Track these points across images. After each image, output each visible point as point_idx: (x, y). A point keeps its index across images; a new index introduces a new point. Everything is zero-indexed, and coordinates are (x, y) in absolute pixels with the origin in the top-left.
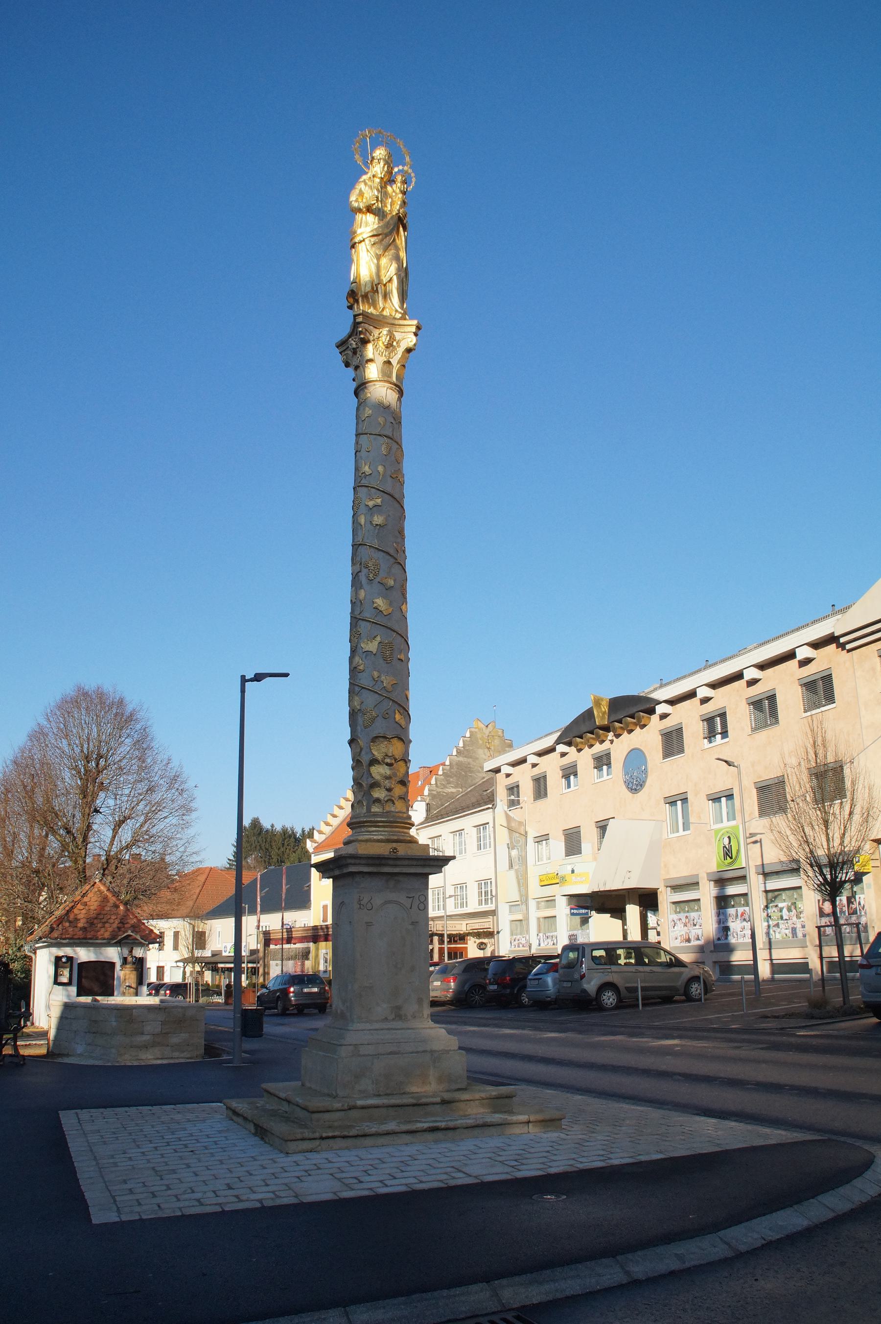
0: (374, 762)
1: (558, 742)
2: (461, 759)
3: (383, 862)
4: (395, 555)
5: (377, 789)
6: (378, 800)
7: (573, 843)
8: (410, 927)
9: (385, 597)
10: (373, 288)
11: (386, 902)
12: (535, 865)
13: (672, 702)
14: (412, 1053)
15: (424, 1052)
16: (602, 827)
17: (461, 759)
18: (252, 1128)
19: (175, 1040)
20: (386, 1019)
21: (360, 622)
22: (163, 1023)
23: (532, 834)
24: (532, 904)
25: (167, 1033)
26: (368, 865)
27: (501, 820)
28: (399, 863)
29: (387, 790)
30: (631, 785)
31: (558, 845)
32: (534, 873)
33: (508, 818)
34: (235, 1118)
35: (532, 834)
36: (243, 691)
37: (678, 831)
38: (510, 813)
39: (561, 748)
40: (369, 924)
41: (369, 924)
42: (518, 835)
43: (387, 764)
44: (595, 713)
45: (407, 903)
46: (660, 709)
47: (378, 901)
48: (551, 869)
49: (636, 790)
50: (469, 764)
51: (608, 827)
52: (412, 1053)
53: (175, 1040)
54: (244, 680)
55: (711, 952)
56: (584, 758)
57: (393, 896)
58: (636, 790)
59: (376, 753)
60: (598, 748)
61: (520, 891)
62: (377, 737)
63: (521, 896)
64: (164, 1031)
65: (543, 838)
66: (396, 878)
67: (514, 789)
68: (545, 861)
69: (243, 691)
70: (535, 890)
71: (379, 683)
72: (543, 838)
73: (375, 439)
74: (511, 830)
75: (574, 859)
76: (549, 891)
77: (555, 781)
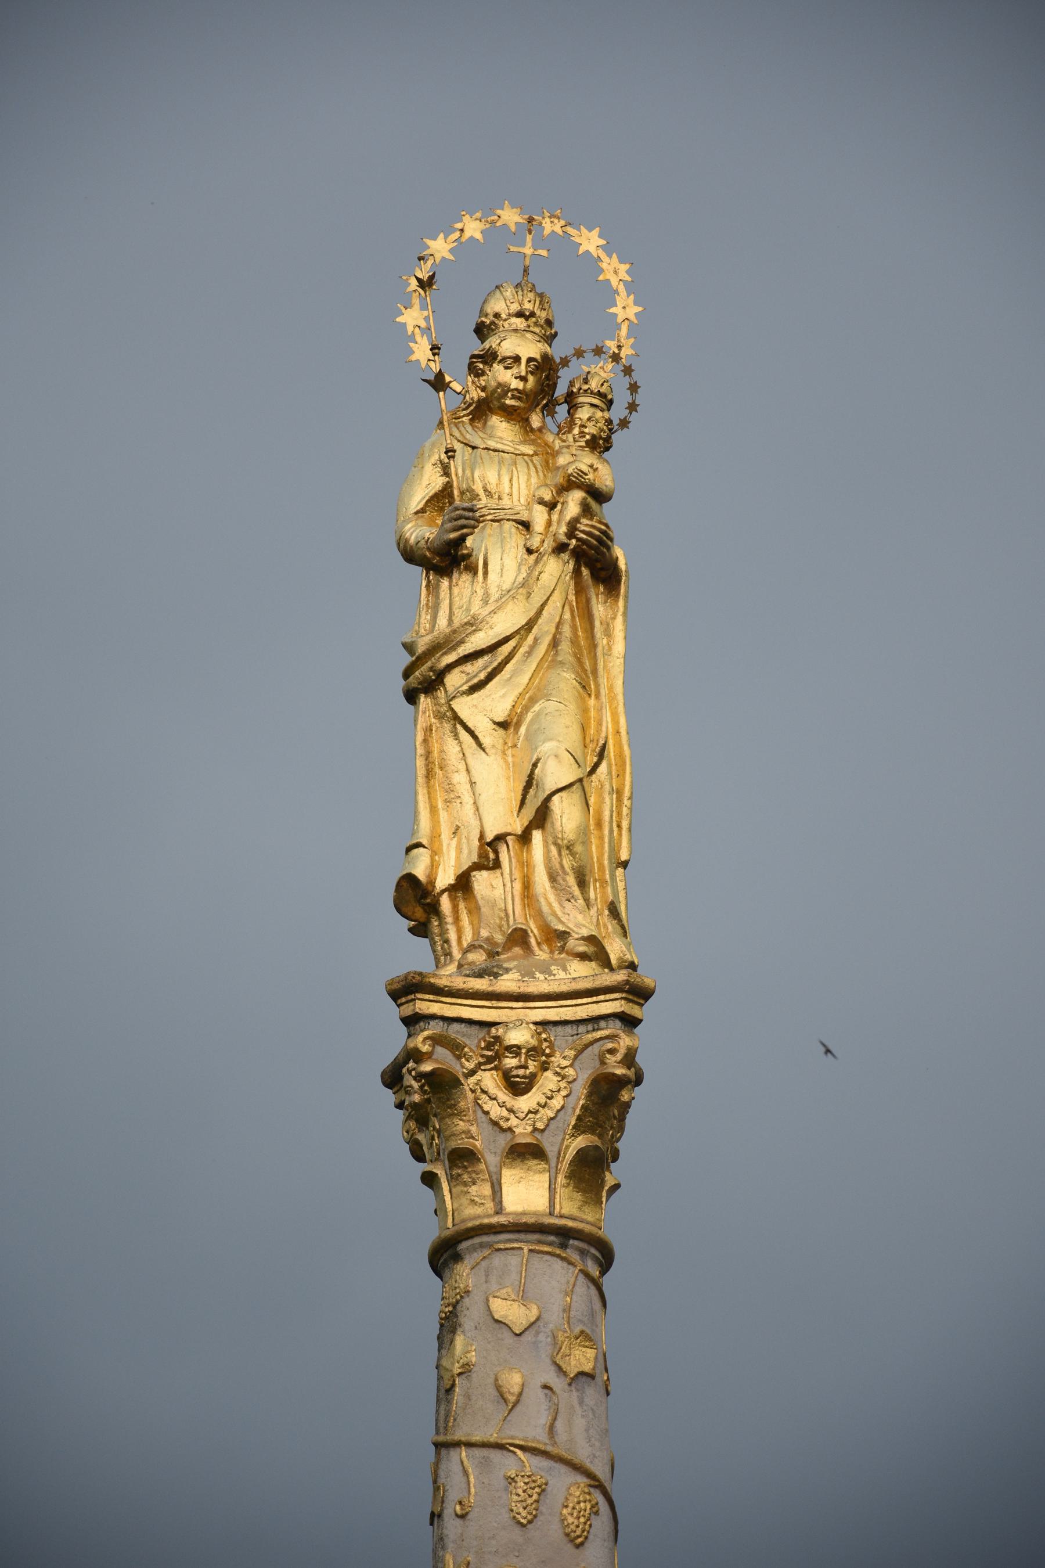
10: (483, 855)
73: (485, 1465)
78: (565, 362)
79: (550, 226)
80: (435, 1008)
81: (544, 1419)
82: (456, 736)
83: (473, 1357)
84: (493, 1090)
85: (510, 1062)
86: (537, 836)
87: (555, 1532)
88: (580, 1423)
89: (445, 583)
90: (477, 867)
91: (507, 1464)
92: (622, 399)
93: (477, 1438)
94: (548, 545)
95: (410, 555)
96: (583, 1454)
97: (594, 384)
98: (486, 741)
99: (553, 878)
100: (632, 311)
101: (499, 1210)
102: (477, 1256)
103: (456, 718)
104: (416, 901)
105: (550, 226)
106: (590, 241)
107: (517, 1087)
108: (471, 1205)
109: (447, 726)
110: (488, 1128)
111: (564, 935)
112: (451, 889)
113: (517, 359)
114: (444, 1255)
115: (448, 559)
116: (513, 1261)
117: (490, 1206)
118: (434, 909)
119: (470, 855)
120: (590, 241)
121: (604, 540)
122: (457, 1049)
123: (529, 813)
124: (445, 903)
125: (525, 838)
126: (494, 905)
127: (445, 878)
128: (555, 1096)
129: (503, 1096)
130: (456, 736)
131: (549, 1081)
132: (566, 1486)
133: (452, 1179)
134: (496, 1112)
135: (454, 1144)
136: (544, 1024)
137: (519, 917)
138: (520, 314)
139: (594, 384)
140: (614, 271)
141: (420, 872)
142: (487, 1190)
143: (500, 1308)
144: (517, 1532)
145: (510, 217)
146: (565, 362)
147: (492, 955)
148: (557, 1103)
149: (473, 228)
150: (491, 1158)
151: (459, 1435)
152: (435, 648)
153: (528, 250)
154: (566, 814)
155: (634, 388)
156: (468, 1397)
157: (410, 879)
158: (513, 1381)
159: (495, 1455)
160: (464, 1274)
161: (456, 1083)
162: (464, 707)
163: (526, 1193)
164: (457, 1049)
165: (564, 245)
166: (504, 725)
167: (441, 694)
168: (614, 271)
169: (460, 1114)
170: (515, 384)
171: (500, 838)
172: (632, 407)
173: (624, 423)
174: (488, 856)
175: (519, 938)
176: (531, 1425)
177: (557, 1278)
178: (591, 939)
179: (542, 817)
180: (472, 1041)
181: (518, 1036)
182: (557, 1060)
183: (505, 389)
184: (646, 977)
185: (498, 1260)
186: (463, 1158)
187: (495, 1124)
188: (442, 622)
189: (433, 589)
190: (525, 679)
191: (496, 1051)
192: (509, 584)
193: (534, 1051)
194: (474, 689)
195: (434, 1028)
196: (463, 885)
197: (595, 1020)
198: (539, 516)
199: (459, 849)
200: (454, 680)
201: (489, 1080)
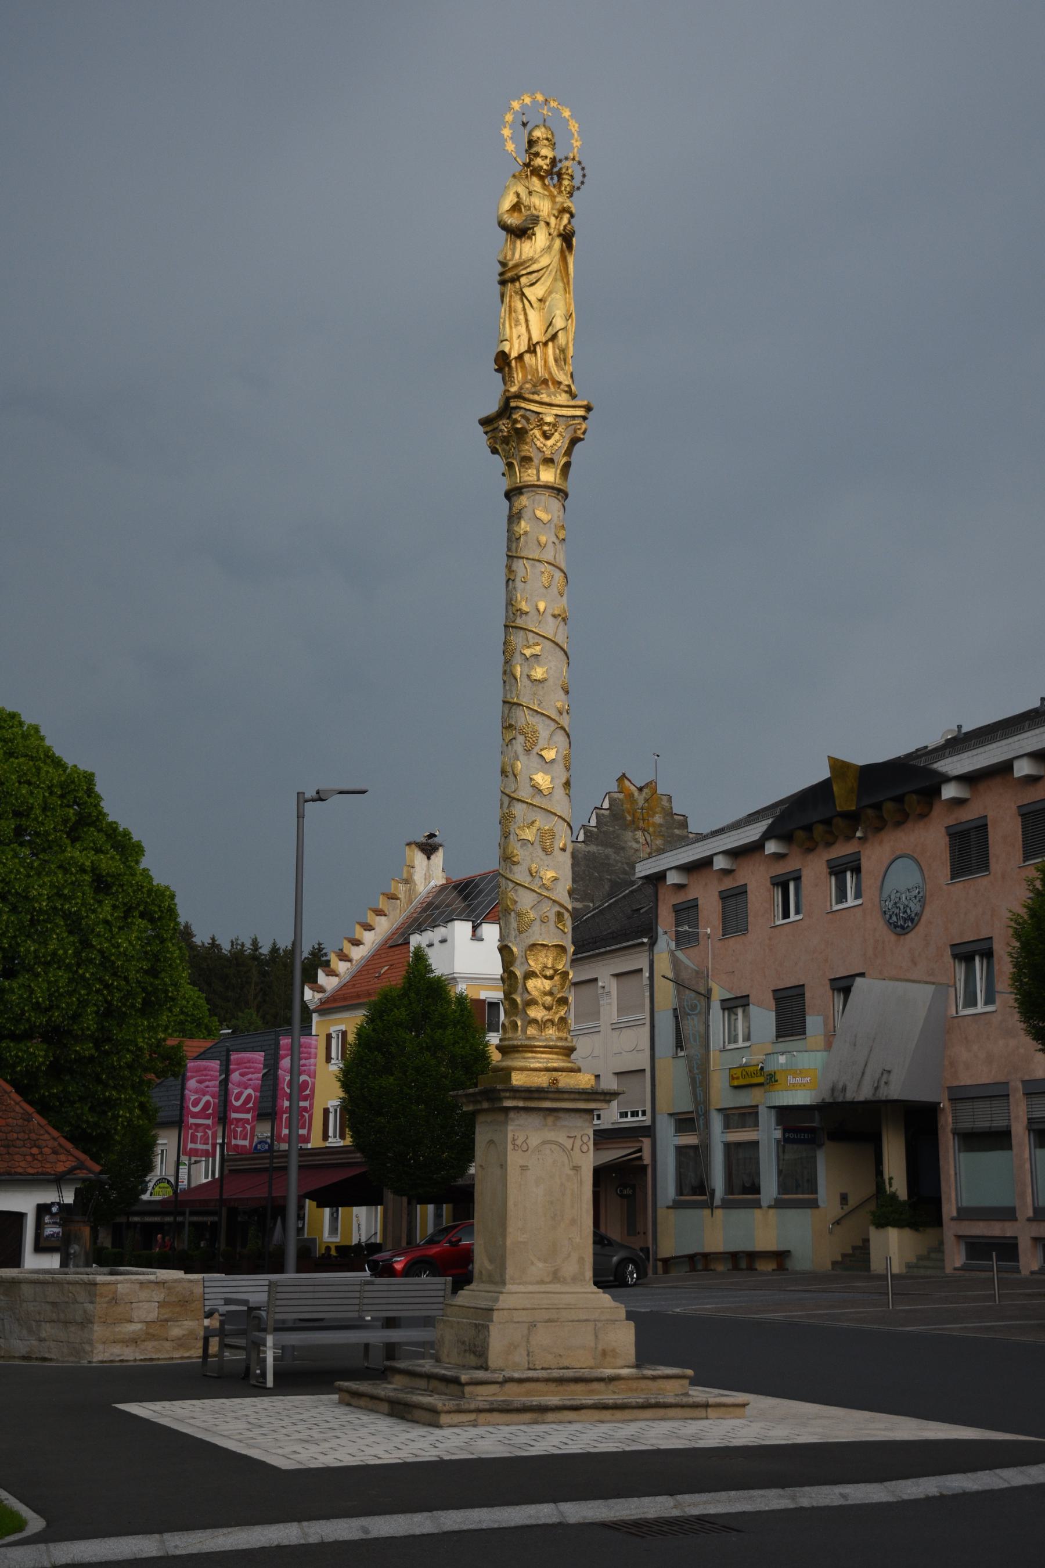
0: (530, 975)
1: (766, 836)
2: (593, 848)
3: (542, 1095)
4: (557, 719)
5: (533, 1007)
6: (534, 1021)
7: (791, 1012)
8: (571, 1173)
9: (546, 773)
10: (529, 347)
11: (544, 1143)
12: (724, 1050)
13: (970, 779)
14: (573, 1321)
15: (586, 1320)
16: (843, 987)
17: (593, 848)
18: (385, 1407)
19: (176, 1331)
20: (542, 1282)
21: (515, 803)
22: (162, 1305)
23: (718, 993)
24: (717, 1122)
25: (167, 1320)
26: (525, 1099)
27: (663, 965)
28: (561, 1096)
29: (545, 1008)
30: (894, 919)
31: (763, 1018)
32: (720, 1066)
33: (676, 963)
34: (354, 1401)
35: (718, 993)
36: (300, 816)
37: (975, 1005)
38: (679, 954)
39: (771, 847)
40: (524, 1168)
41: (524, 1168)
42: (693, 995)
43: (546, 977)
44: (835, 788)
45: (568, 1143)
46: (949, 791)
47: (534, 1140)
48: (755, 1058)
49: (902, 927)
50: (607, 857)
51: (853, 989)
52: (573, 1321)
53: (176, 1331)
54: (302, 800)
55: (1029, 1220)
56: (814, 870)
57: (551, 1135)
58: (902, 927)
59: (532, 963)
60: (842, 850)
61: (695, 1094)
62: (534, 945)
63: (697, 1103)
64: (162, 1317)
65: (735, 1004)
66: (555, 1114)
67: (687, 912)
68: (741, 1044)
69: (300, 816)
70: (721, 1095)
71: (537, 878)
72: (735, 1004)
73: (533, 566)
74: (679, 983)
75: (792, 1044)
76: (746, 1099)
77: (760, 895)
78: (560, 161)
79: (553, 104)
80: (523, 405)
81: (553, 553)
82: (522, 301)
83: (528, 529)
84: (538, 436)
85: (546, 428)
86: (550, 344)
87: (556, 591)
88: (562, 556)
89: (518, 242)
90: (526, 352)
91: (542, 567)
92: (578, 178)
93: (530, 557)
94: (555, 233)
95: (504, 227)
96: (563, 566)
97: (570, 171)
98: (535, 305)
99: (556, 360)
100: (578, 144)
101: (538, 479)
102: (530, 494)
103: (523, 294)
104: (503, 361)
105: (553, 104)
106: (566, 114)
107: (547, 437)
108: (529, 476)
109: (518, 297)
110: (536, 450)
111: (560, 383)
112: (516, 358)
113: (546, 157)
114: (512, 493)
115: (522, 233)
116: (543, 498)
117: (535, 478)
118: (509, 365)
119: (524, 347)
120: (566, 114)
121: (573, 234)
122: (528, 420)
123: (549, 335)
124: (513, 363)
125: (545, 344)
126: (531, 366)
127: (514, 354)
128: (557, 442)
129: (542, 439)
130: (522, 301)
131: (557, 436)
132: (558, 575)
133: (521, 466)
134: (539, 444)
135: (523, 454)
136: (557, 415)
137: (542, 372)
138: (547, 139)
139: (570, 171)
140: (574, 126)
141: (507, 350)
142: (535, 472)
143: (539, 514)
144: (544, 590)
145: (540, 98)
146: (560, 161)
147: (534, 386)
148: (559, 444)
149: (527, 100)
150: (536, 461)
151: (522, 555)
152: (516, 266)
153: (545, 112)
154: (561, 338)
155: (584, 176)
156: (526, 542)
157: (503, 353)
158: (543, 539)
159: (537, 564)
160: (524, 500)
161: (527, 432)
162: (526, 291)
163: (548, 476)
164: (528, 420)
165: (557, 112)
166: (540, 300)
167: (517, 284)
168: (574, 126)
169: (526, 444)
170: (545, 167)
171: (538, 343)
172: (582, 183)
173: (578, 188)
174: (532, 349)
175: (545, 382)
176: (548, 555)
177: (555, 504)
178: (569, 386)
179: (554, 337)
180: (533, 418)
181: (549, 419)
182: (560, 429)
183: (541, 167)
184: (592, 405)
185: (537, 497)
186: (527, 460)
187: (538, 449)
188: (517, 256)
189: (514, 243)
190: (548, 284)
191: (541, 423)
192: (539, 247)
193: (554, 425)
194: (532, 285)
195: (522, 412)
196: (520, 357)
197: (574, 417)
198: (553, 221)
199: (520, 344)
200: (524, 280)
201: (537, 432)
